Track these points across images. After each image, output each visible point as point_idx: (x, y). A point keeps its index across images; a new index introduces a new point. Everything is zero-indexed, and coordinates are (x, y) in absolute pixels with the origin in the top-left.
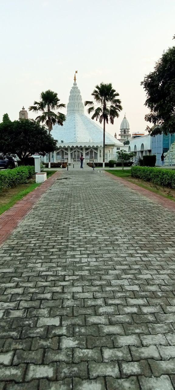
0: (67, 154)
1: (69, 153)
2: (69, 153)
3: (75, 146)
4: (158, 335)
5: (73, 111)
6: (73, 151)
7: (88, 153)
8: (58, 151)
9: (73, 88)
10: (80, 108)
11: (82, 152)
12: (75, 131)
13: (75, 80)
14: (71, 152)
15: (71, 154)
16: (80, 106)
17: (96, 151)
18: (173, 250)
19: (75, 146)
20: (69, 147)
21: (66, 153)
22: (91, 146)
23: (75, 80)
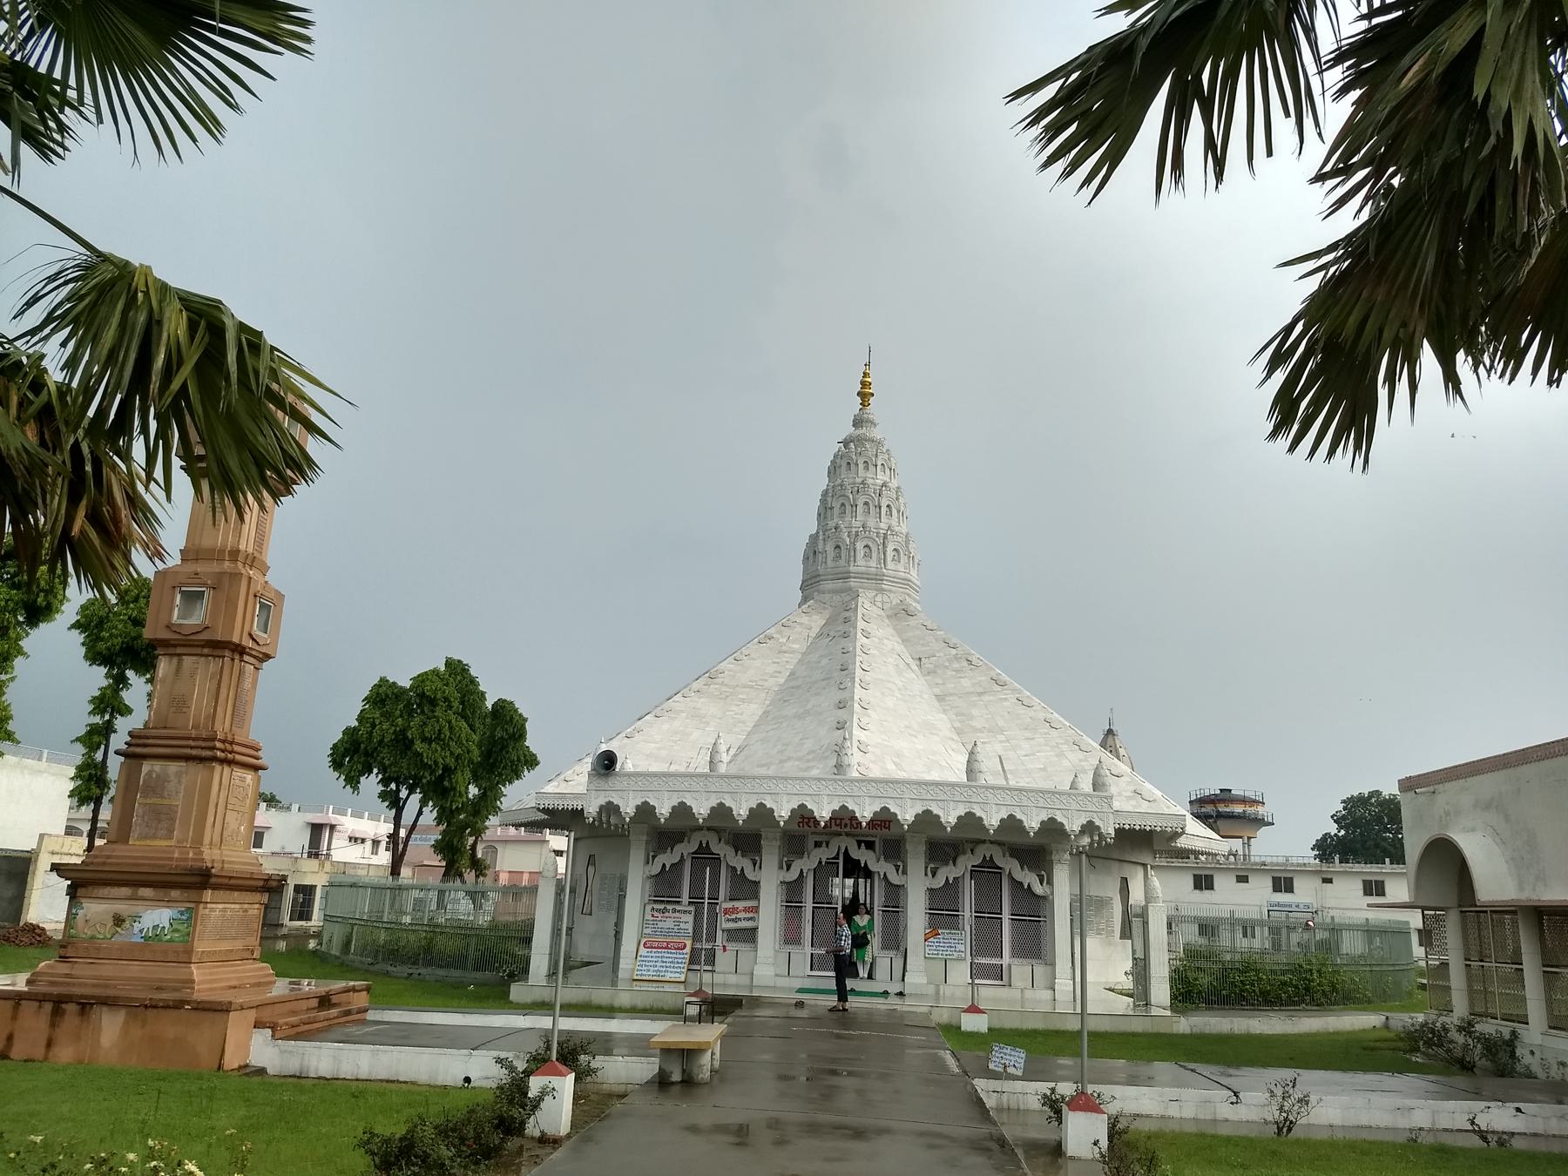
0: (747, 889)
1: (770, 879)
2: (770, 879)
3: (823, 812)
4: (1434, 1122)
5: (839, 584)
6: (806, 864)
7: (952, 888)
8: (668, 859)
9: (846, 443)
10: (890, 565)
11: (895, 878)
12: (841, 705)
13: (864, 396)
14: (793, 875)
15: (792, 891)
16: (890, 554)
17: (1028, 878)
18: (694, 1129)
19: (823, 812)
20: (761, 814)
21: (738, 878)
22: (992, 820)
23: (864, 396)
